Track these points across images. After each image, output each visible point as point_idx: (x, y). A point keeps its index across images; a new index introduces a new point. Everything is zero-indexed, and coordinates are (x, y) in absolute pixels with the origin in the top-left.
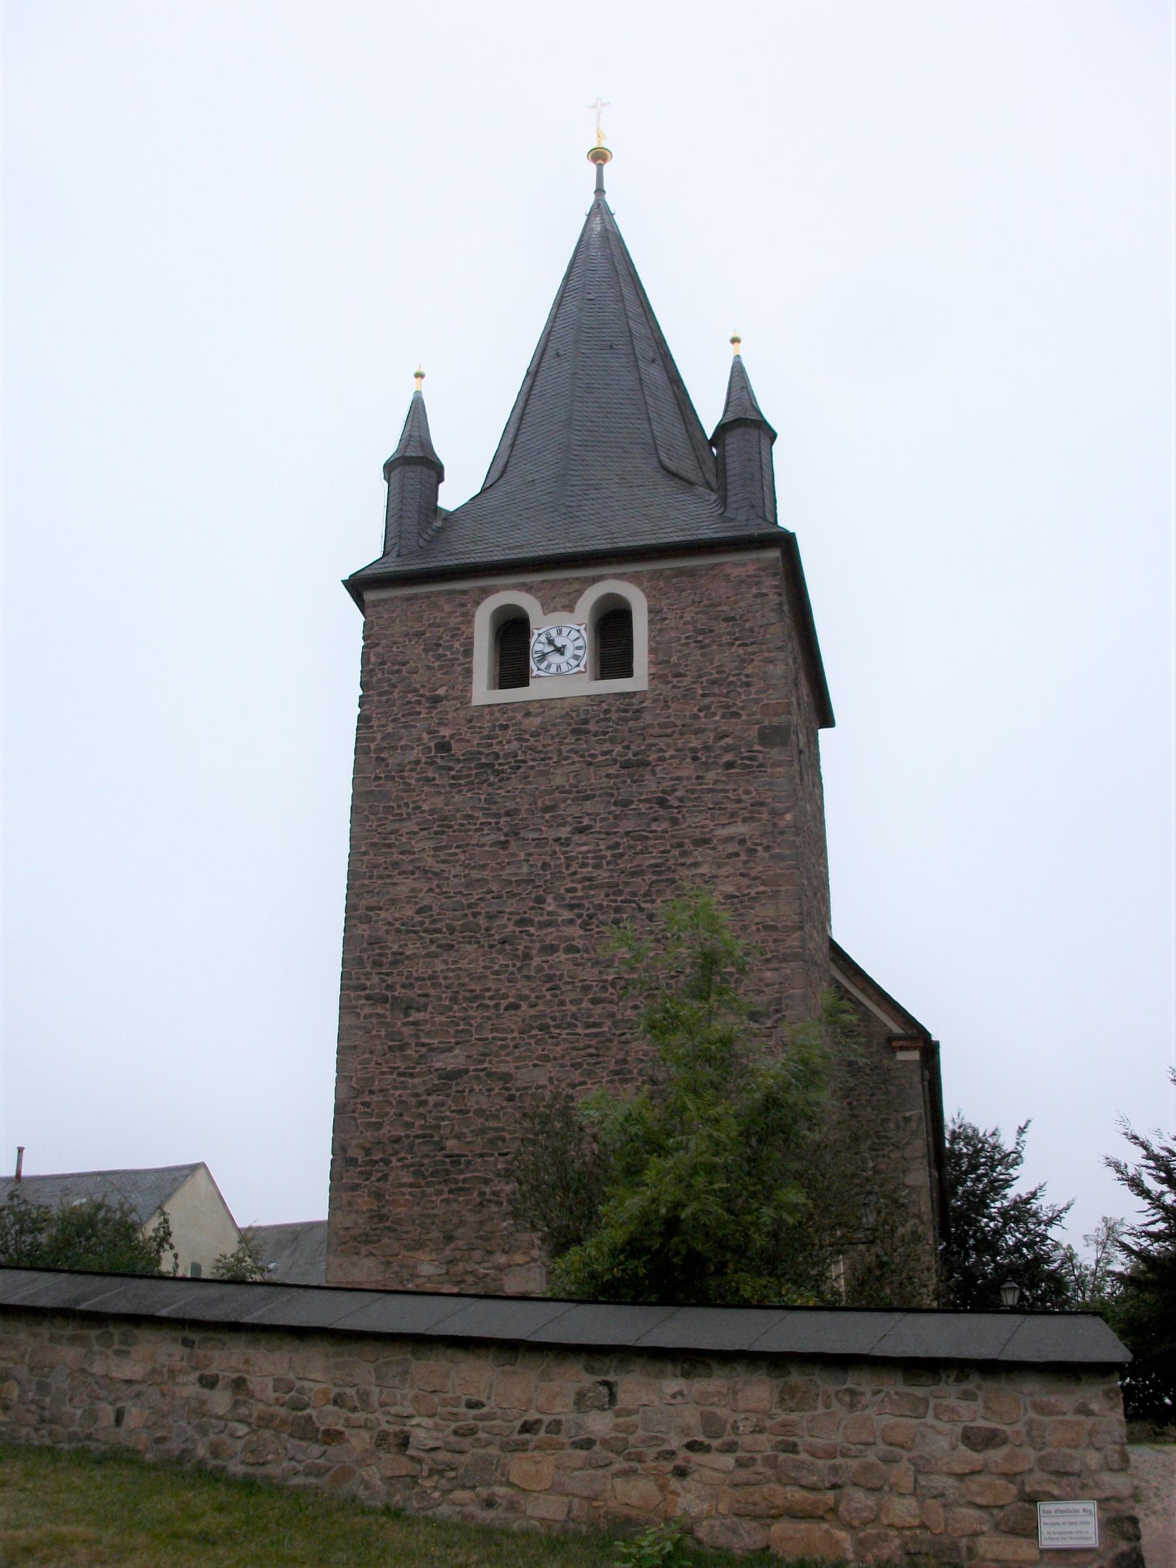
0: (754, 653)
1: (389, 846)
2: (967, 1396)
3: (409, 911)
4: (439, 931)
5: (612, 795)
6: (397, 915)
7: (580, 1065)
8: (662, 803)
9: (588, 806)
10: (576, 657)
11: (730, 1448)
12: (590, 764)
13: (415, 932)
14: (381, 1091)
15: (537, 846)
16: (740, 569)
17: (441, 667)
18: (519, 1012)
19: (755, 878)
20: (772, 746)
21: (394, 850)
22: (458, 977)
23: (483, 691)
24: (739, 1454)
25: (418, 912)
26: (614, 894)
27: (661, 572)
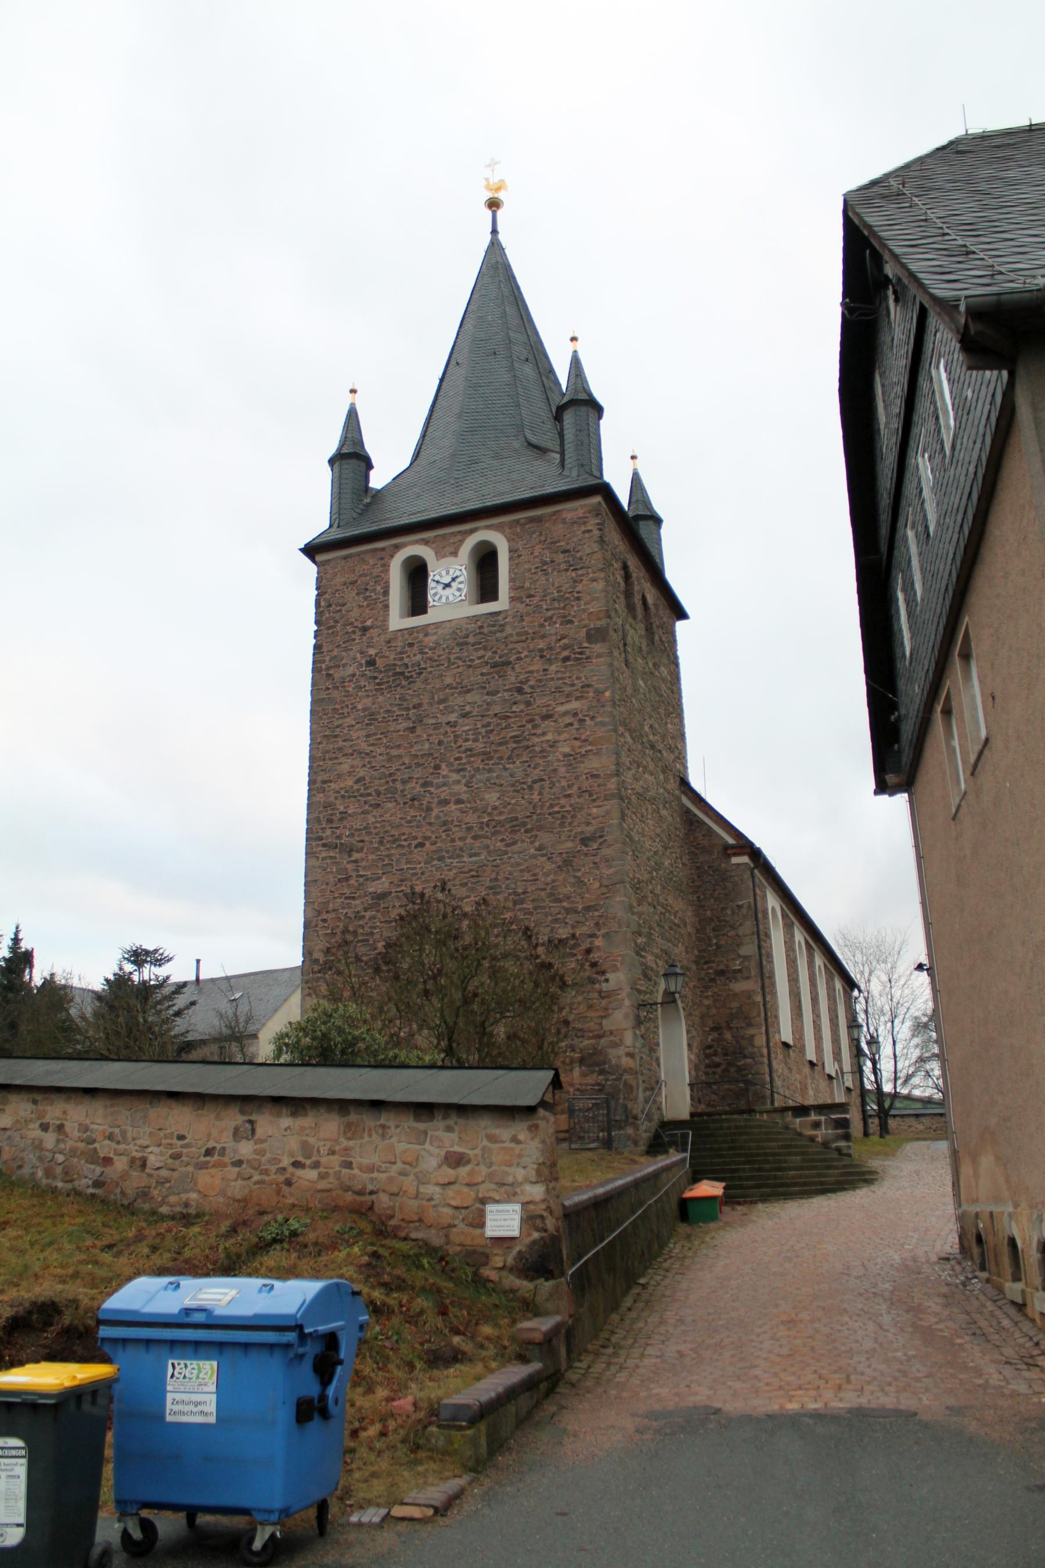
0: (582, 575)
1: (336, 736)
2: (449, 1129)
3: (350, 782)
4: (369, 795)
5: (485, 688)
6: (342, 786)
7: (466, 884)
8: (520, 691)
9: (469, 697)
10: (459, 590)
11: (316, 1165)
12: (470, 666)
13: (355, 797)
14: (334, 910)
15: (434, 729)
16: (573, 513)
17: (368, 605)
18: (424, 849)
19: (585, 741)
20: (596, 642)
21: (339, 739)
22: (384, 826)
23: (397, 620)
24: (322, 1170)
25: (357, 782)
26: (488, 759)
27: (517, 521)
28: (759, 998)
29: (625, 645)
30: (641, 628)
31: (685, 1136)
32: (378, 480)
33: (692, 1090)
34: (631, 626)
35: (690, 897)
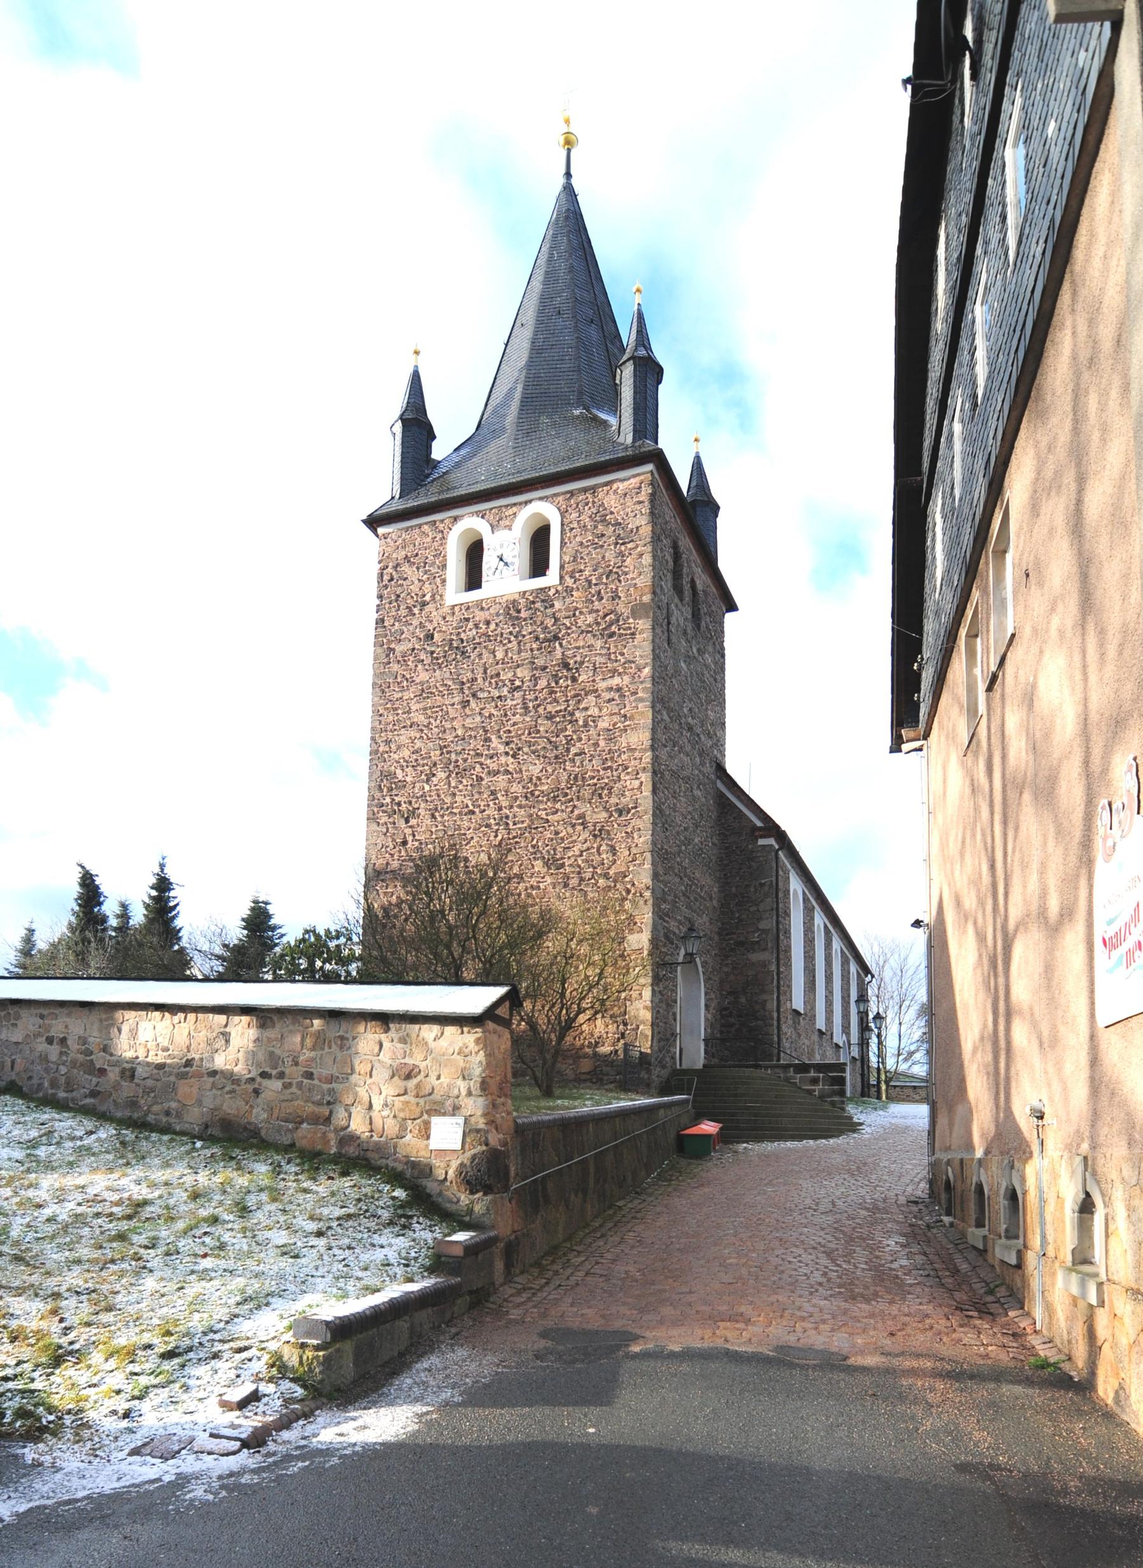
11: (281, 1075)
23: (454, 594)
28: (773, 968)
29: (669, 623)
30: (687, 612)
31: (690, 1082)
32: (440, 450)
33: (706, 1045)
34: (677, 606)
35: (718, 874)
